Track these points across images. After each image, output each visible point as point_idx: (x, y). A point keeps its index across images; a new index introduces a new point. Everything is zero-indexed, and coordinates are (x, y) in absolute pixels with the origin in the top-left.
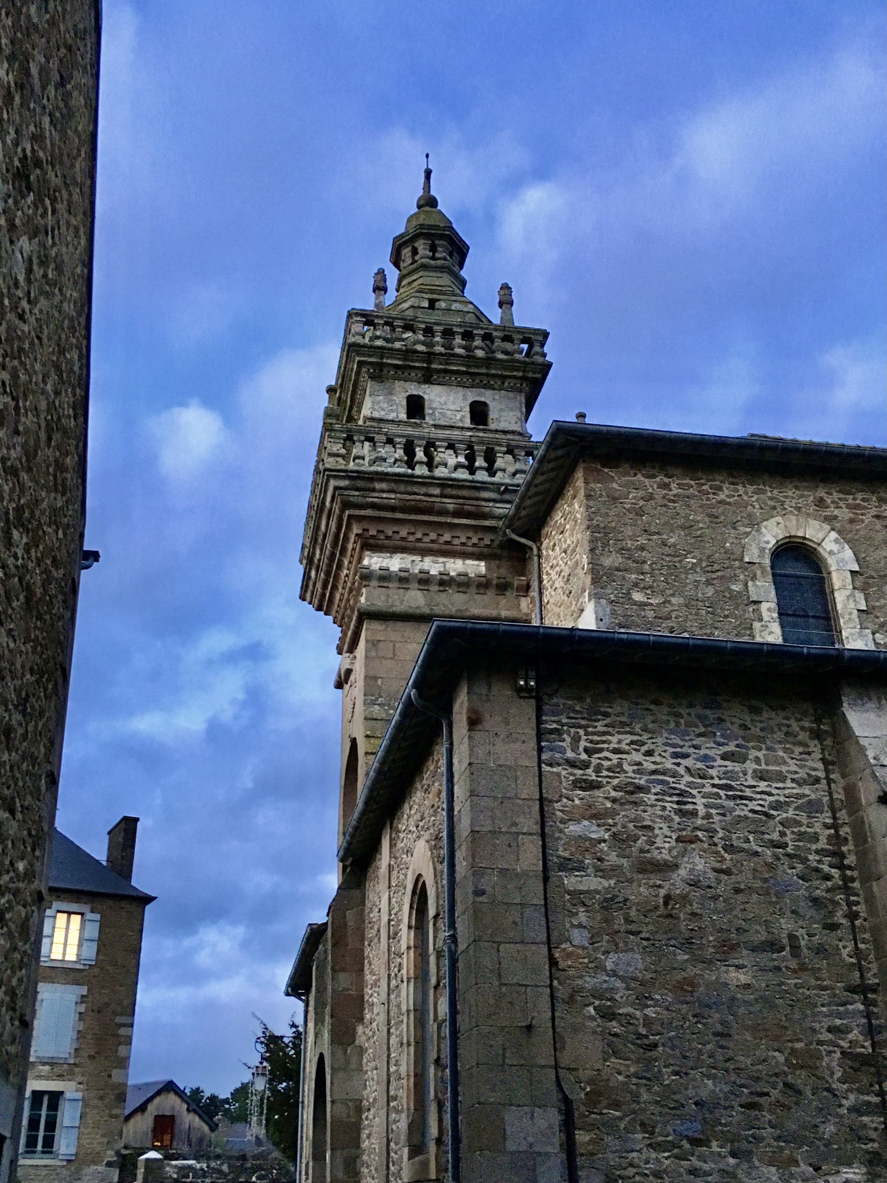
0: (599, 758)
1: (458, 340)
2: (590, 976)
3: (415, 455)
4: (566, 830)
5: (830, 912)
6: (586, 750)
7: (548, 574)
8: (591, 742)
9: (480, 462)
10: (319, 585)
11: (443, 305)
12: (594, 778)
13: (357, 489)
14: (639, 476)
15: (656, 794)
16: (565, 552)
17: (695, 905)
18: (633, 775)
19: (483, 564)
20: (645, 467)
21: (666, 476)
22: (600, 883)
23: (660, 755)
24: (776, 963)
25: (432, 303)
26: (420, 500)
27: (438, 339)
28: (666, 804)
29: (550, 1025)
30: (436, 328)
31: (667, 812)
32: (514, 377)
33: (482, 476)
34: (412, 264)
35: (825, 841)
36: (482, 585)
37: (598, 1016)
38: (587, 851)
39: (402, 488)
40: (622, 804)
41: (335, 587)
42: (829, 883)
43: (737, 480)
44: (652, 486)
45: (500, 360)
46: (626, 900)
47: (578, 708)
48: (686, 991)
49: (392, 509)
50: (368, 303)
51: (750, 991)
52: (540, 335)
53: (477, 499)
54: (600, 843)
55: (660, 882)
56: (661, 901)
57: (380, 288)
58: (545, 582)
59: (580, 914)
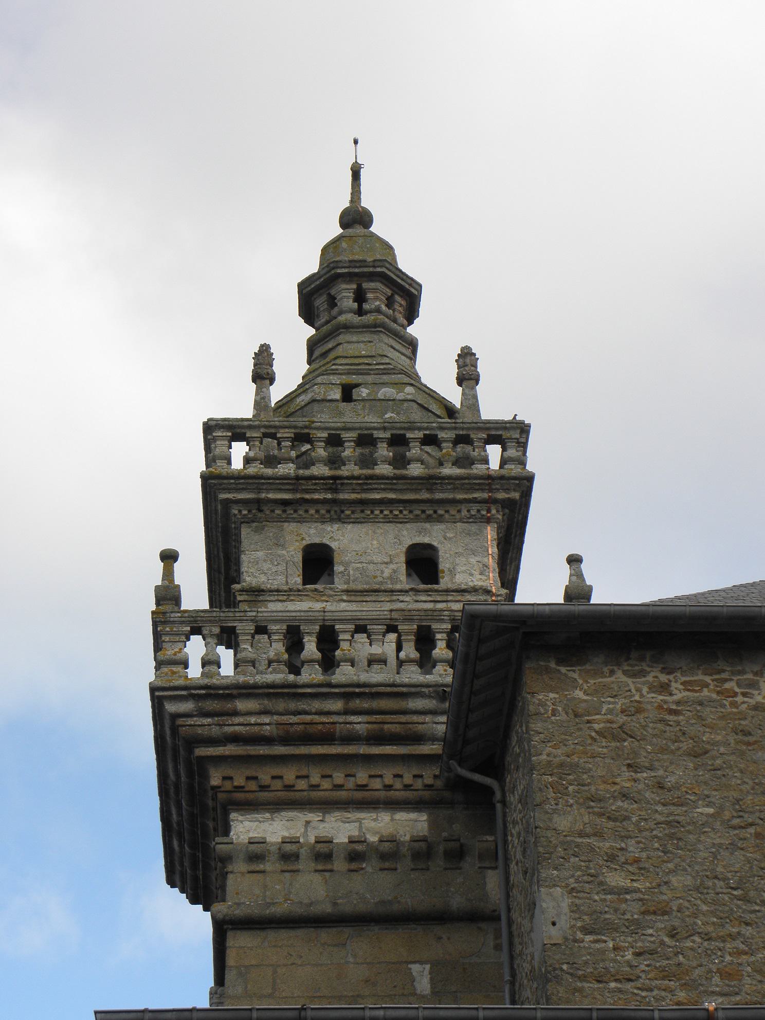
1: (383, 451)
19: (424, 817)
20: (628, 659)
21: (663, 670)
25: (347, 394)
26: (311, 723)
30: (345, 435)
32: (475, 501)
34: (327, 322)
36: (422, 852)
39: (281, 705)
44: (639, 690)
45: (449, 478)
49: (268, 740)
50: (241, 406)
52: (514, 428)
57: (263, 373)
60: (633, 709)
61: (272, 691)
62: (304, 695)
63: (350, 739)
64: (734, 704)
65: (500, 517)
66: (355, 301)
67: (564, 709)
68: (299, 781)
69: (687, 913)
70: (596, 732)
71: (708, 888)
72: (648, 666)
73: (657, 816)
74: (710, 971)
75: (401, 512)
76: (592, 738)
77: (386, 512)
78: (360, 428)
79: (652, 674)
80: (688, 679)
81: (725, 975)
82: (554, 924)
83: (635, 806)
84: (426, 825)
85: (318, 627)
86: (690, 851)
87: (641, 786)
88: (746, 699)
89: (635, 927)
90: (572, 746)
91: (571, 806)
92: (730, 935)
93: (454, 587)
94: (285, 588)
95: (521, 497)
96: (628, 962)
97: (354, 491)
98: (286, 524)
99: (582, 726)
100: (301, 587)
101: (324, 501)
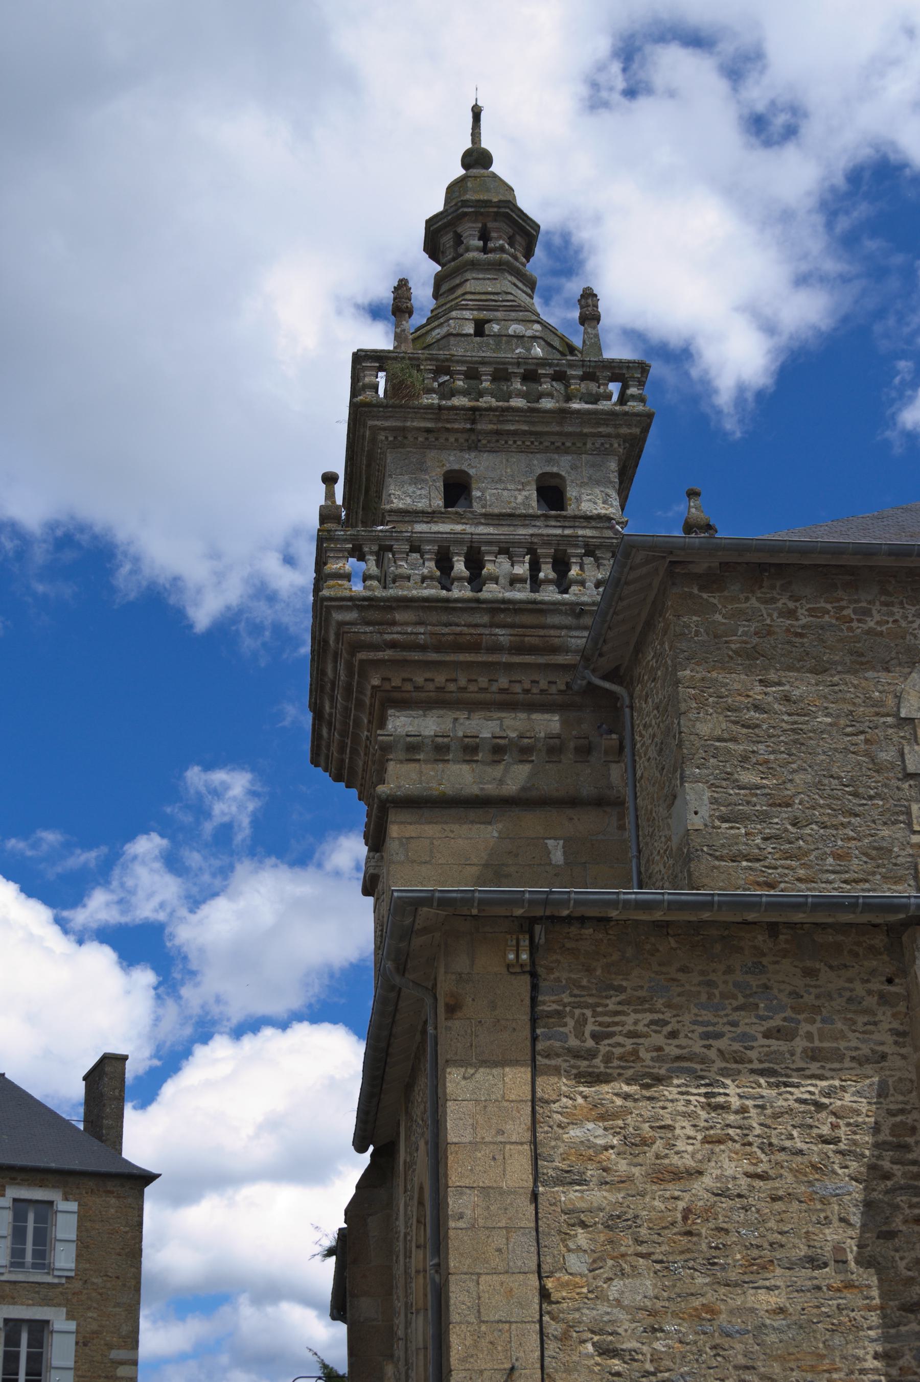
0: (609, 1045)
2: (588, 1308)
3: (452, 568)
4: (565, 1136)
5: (887, 1218)
6: (595, 1036)
7: (641, 736)
8: (601, 1024)
9: (547, 572)
10: (334, 748)
11: (496, 328)
12: (602, 1069)
13: (368, 623)
14: (754, 602)
15: (679, 1086)
16: (657, 708)
17: (721, 1218)
18: (651, 1064)
20: (761, 587)
21: (791, 598)
22: (605, 1198)
23: (686, 1036)
24: (815, 1282)
26: (460, 634)
27: (486, 384)
28: (692, 1098)
29: (538, 1365)
30: (482, 369)
31: (692, 1108)
33: (549, 594)
34: (454, 259)
35: (887, 1132)
36: (554, 748)
37: (596, 1353)
38: (590, 1160)
39: (434, 617)
40: (636, 1100)
41: (354, 751)
42: (889, 1183)
43: (892, 599)
44: (770, 615)
45: (578, 411)
46: (636, 1217)
47: (584, 982)
48: (704, 1319)
49: (423, 648)
50: (379, 338)
51: (782, 1316)
53: (543, 627)
54: (606, 1150)
55: (680, 1193)
56: (679, 1216)
58: (638, 745)
59: (580, 1236)
60: (764, 632)
61: (427, 604)
62: (454, 609)
63: (496, 648)
64: (850, 629)
65: (621, 450)
66: (479, 239)
67: (705, 631)
68: (448, 684)
69: (807, 805)
70: (733, 651)
71: (825, 785)
72: (779, 594)
73: (784, 725)
74: (826, 853)
75: (532, 443)
76: (729, 656)
77: (519, 443)
78: (498, 363)
79: (781, 601)
80: (812, 606)
81: (838, 857)
82: (696, 813)
83: (765, 716)
84: (558, 725)
85: (465, 548)
86: (810, 754)
87: (770, 699)
88: (860, 625)
89: (764, 817)
90: (712, 663)
91: (711, 715)
92: (842, 824)
93: (581, 513)
94: (430, 510)
95: (641, 432)
96: (757, 845)
97: (491, 422)
98: (428, 451)
99: (720, 645)
100: (443, 510)
101: (464, 431)
